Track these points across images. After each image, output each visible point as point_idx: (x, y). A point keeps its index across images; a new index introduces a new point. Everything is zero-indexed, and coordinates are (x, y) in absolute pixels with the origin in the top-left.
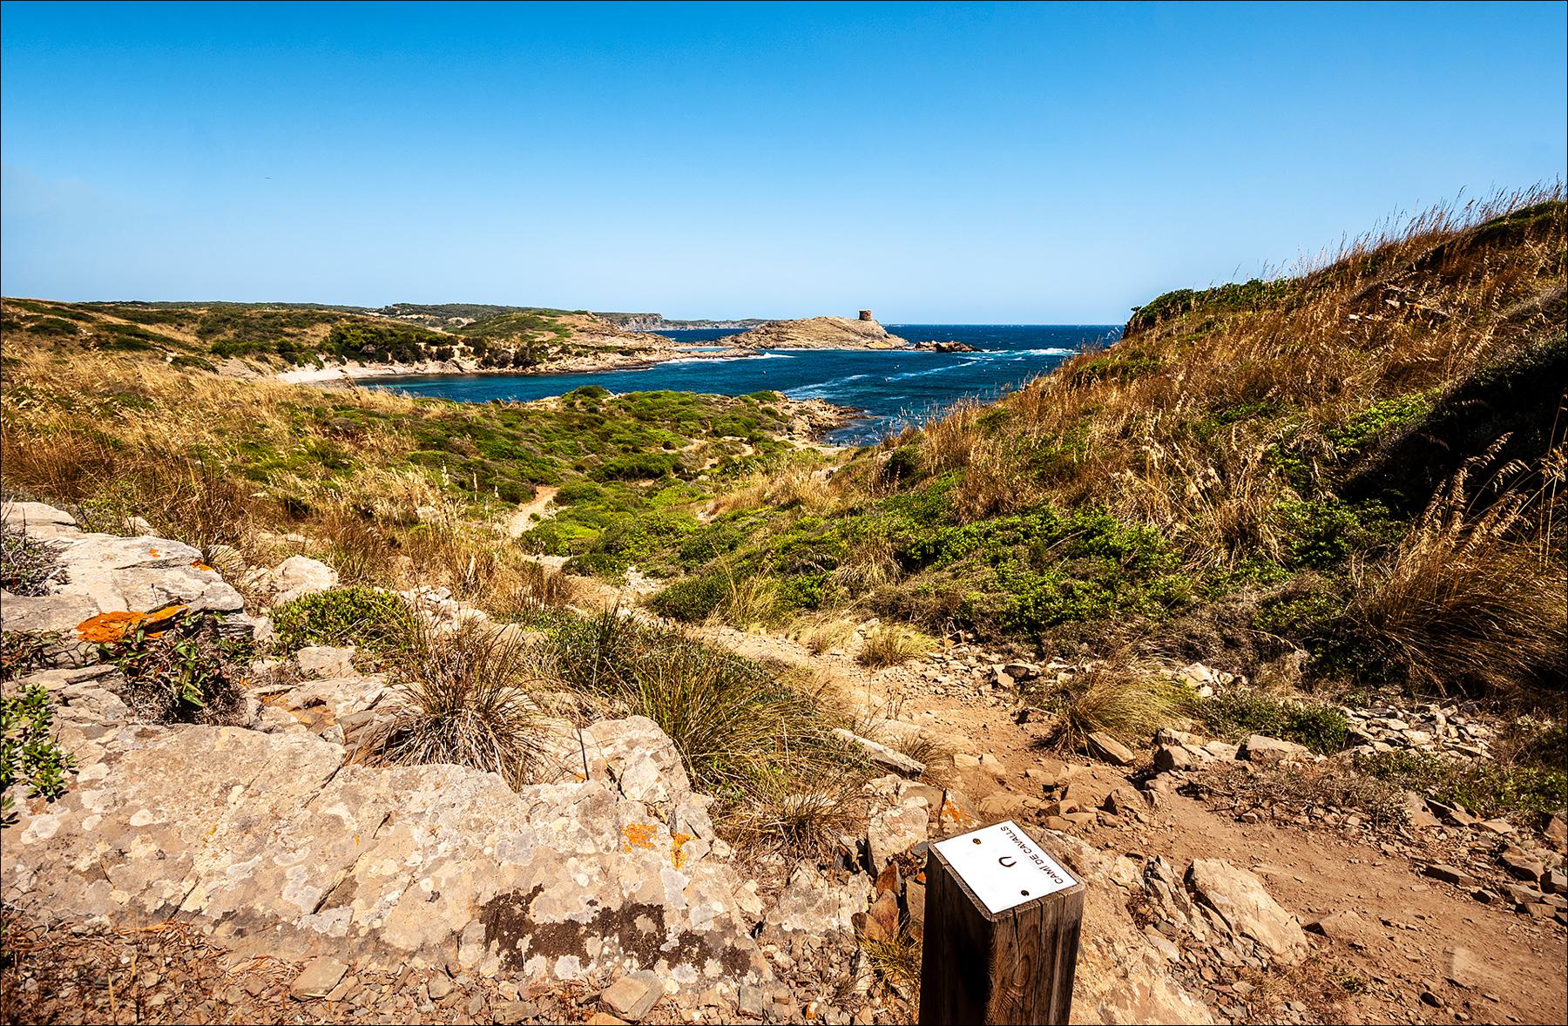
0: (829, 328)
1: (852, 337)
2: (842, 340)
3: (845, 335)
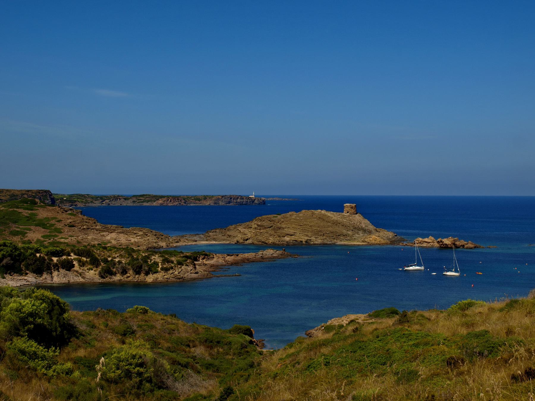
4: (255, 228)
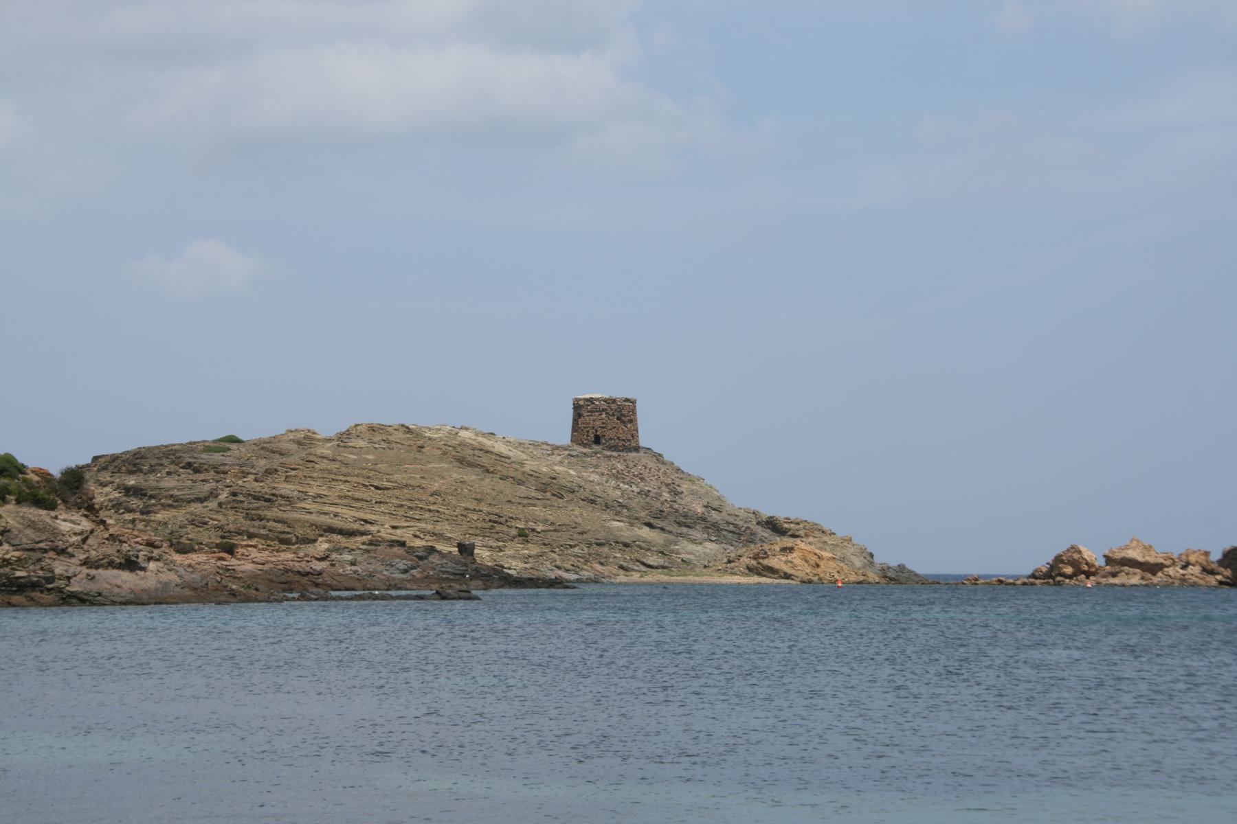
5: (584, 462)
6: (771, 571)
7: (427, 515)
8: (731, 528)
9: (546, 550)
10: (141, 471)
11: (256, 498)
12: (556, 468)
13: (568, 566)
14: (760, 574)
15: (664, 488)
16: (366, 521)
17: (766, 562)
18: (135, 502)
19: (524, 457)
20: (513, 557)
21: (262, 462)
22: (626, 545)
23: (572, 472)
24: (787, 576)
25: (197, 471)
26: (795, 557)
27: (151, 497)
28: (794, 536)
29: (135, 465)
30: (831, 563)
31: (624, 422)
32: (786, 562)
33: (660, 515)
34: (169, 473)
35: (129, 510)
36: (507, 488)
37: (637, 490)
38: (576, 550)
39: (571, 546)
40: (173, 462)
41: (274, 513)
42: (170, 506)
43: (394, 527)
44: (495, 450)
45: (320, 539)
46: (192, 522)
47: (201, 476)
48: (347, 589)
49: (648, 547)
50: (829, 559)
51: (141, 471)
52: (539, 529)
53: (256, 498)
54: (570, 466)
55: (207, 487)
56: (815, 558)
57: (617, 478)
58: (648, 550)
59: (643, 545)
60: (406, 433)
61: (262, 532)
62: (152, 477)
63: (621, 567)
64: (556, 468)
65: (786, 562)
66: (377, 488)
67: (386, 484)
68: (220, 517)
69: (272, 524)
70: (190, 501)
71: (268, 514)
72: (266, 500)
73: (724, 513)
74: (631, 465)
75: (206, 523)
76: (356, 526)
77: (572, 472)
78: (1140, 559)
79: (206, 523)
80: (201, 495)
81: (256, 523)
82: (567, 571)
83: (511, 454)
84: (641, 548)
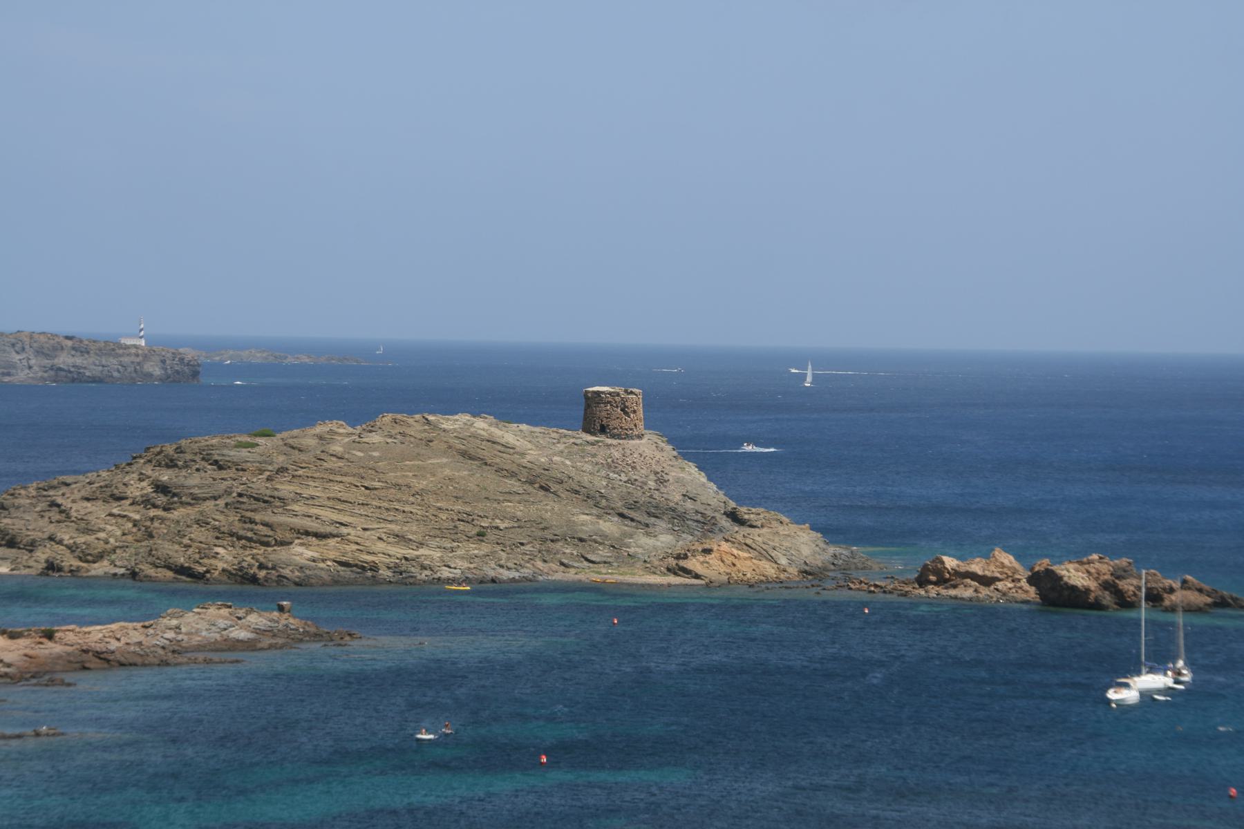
0: (465, 474)
1: (585, 520)
2: (548, 538)
3: (550, 509)
4: (147, 502)
5: (583, 451)
6: (686, 572)
7: (400, 517)
8: (699, 517)
9: (498, 548)
10: (176, 466)
11: (256, 499)
12: (556, 458)
13: (510, 565)
14: (676, 574)
15: (652, 477)
16: (342, 524)
17: (682, 563)
18: (161, 499)
19: (529, 446)
20: (462, 558)
21: (281, 458)
22: (581, 540)
23: (568, 462)
24: (697, 576)
25: (221, 468)
26: (712, 559)
27: (175, 495)
28: (752, 526)
29: (172, 461)
30: (748, 563)
31: (626, 414)
32: (702, 563)
33: (634, 506)
34: (198, 470)
35: (155, 506)
36: (491, 481)
37: (624, 478)
38: (528, 547)
39: (522, 544)
40: (203, 459)
41: (268, 516)
42: (189, 504)
43: (365, 529)
44: (503, 441)
45: (297, 541)
46: (197, 522)
47: (224, 474)
48: (369, 553)
49: (600, 539)
50: (746, 559)
51: (176, 466)
52: (502, 526)
53: (256, 499)
54: (570, 455)
55: (224, 486)
56: (732, 559)
57: (609, 467)
58: (600, 544)
59: (599, 539)
60: (424, 424)
61: (249, 534)
62: (184, 473)
63: (562, 564)
64: (556, 458)
65: (702, 563)
66: (367, 488)
67: (377, 484)
68: (221, 518)
69: (260, 527)
70: (205, 499)
71: (258, 517)
72: (265, 502)
73: (698, 502)
74: (628, 452)
75: (208, 524)
76: (329, 529)
77: (568, 462)
78: (980, 573)
79: (208, 524)
80: (216, 494)
81: (248, 526)
82: (509, 569)
83: (518, 444)
84: (596, 542)
